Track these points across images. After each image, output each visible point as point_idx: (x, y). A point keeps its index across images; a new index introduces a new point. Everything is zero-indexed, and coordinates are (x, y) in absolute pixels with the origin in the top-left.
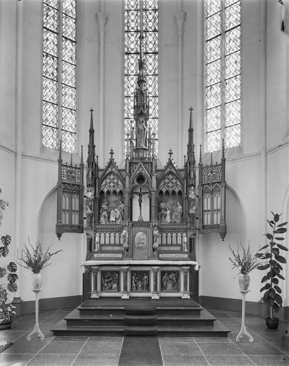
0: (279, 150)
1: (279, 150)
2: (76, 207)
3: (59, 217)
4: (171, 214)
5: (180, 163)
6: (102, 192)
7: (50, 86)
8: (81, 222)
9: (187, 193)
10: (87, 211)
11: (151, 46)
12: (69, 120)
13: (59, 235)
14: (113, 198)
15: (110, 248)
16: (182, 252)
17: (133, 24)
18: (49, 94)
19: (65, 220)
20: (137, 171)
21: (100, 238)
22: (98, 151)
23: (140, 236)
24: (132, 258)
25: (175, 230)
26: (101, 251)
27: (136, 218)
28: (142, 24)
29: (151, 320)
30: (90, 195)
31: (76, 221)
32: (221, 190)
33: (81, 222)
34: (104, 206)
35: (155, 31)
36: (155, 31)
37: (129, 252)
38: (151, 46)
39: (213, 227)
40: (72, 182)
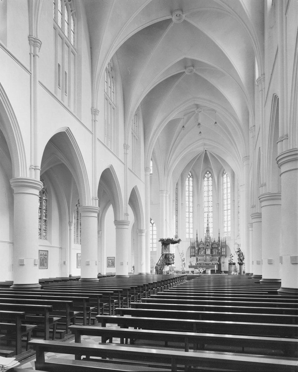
0: (117, 46)
1: (117, 46)
2: (194, 251)
3: (191, 254)
4: (215, 252)
5: (217, 240)
6: (199, 248)
7: (187, 224)
8: (195, 254)
9: (218, 248)
10: (196, 252)
11: (211, 210)
12: (191, 231)
13: (191, 257)
14: (202, 249)
15: (201, 260)
16: (217, 260)
17: (206, 205)
18: (187, 226)
19: (192, 254)
20: (207, 244)
21: (199, 258)
22: (198, 239)
23: (208, 257)
24: (206, 262)
25: (216, 256)
26: (199, 261)
27: (207, 253)
28: (208, 205)
29: (166, 346)
30: (197, 249)
31: (194, 254)
32: (289, 139)
33: (195, 254)
34: (200, 251)
35: (212, 206)
36: (212, 206)
37: (205, 261)
38: (211, 210)
39: (224, 255)
40: (193, 246)
